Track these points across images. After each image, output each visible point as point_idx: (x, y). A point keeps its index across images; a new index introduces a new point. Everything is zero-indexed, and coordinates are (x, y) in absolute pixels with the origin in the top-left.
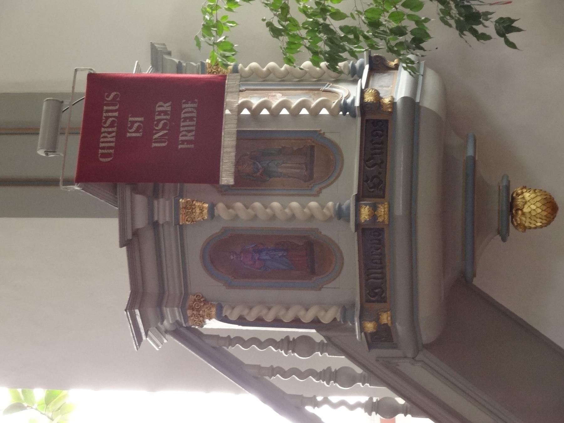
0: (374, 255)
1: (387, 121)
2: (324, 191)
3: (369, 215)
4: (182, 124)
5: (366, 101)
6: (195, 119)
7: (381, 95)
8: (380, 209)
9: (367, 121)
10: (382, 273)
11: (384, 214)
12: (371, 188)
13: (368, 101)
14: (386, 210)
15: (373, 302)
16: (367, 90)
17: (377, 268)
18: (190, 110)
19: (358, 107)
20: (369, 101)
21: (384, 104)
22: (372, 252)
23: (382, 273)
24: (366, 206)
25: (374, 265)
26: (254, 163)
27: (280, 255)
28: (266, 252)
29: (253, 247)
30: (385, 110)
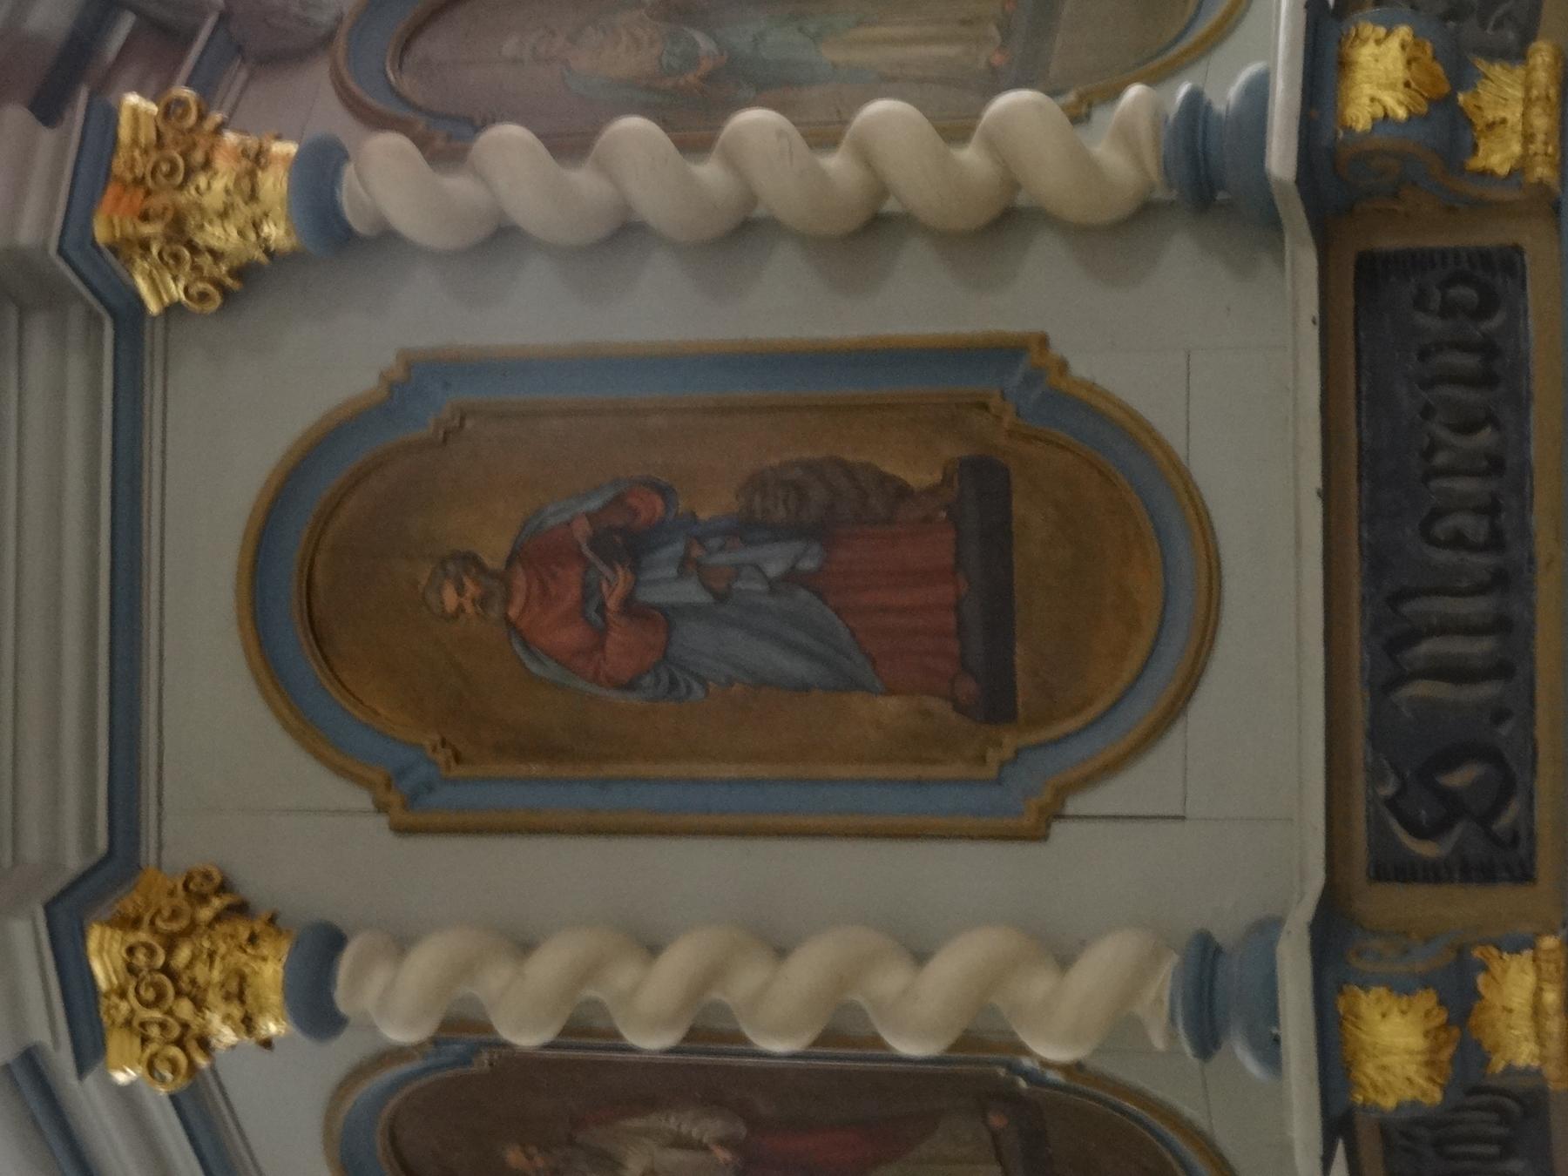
0: (1450, 472)
10: (1501, 625)
15: (1432, 874)
17: (1464, 584)
22: (1428, 453)
23: (1501, 625)
25: (1443, 556)
27: (774, 569)
28: (678, 548)
29: (590, 516)
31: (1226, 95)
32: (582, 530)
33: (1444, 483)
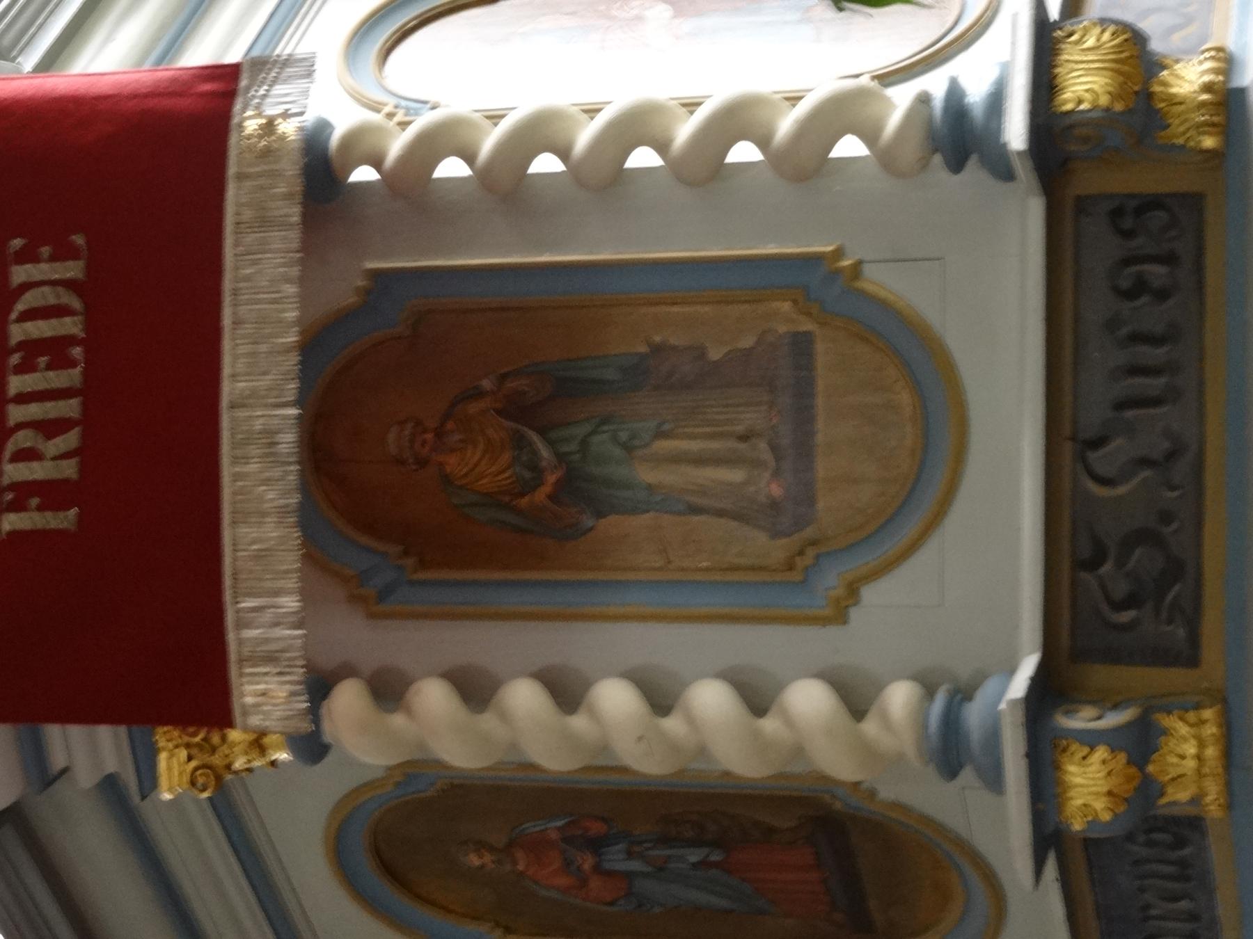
1: (1194, 202)
2: (870, 594)
3: (1110, 793)
4: (16, 384)
5: (1069, 107)
6: (77, 352)
7: (1156, 45)
8: (1172, 743)
9: (1083, 205)
11: (1200, 774)
12: (1119, 606)
13: (1080, 102)
14: (1211, 752)
16: (1071, 35)
18: (52, 301)
19: (1019, 153)
20: (1082, 107)
21: (1174, 101)
24: (1092, 748)
26: (519, 442)
27: (693, 859)
29: (559, 829)
30: (1181, 141)
31: (976, 93)
32: (554, 835)
33: (1156, 923)
